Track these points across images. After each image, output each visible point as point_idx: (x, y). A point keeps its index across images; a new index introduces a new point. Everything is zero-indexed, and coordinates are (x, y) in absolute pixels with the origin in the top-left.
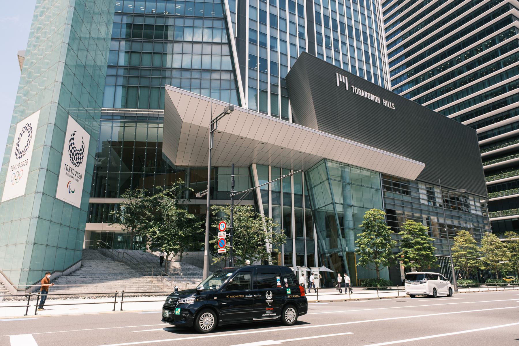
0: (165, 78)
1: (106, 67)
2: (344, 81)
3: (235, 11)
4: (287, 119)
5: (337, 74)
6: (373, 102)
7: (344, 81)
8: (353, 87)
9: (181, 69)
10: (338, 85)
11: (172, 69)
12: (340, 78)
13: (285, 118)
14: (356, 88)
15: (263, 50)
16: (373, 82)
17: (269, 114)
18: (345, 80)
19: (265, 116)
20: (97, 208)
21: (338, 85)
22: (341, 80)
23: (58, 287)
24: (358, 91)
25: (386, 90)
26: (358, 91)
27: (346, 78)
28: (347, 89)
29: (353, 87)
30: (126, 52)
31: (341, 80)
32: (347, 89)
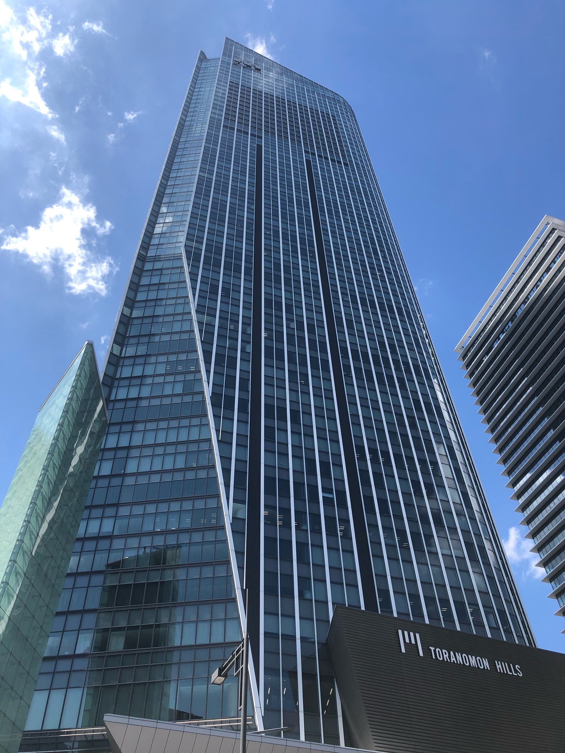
0: (170, 681)
3: (252, 261)
5: (400, 632)
6: (476, 670)
7: (413, 642)
8: (432, 649)
10: (403, 650)
11: (181, 648)
12: (405, 637)
14: (437, 650)
16: (528, 645)
17: (323, 742)
18: (417, 639)
20: (213, 564)
21: (403, 650)
22: (407, 641)
24: (443, 655)
25: (521, 647)
26: (443, 655)
27: (417, 635)
28: (421, 654)
29: (432, 649)
32: (421, 654)
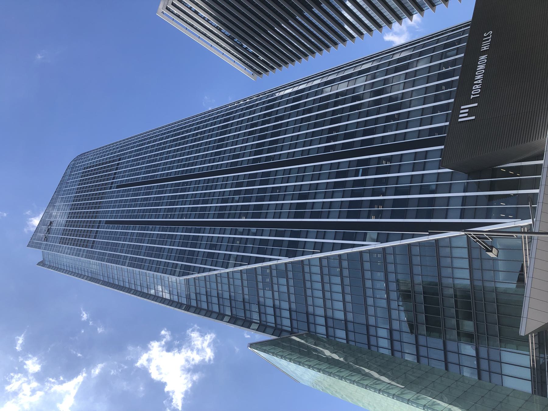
1: (480, 381)
2: (467, 110)
5: (460, 120)
7: (467, 110)
8: (472, 96)
9: (471, 269)
10: (473, 118)
11: (472, 279)
13: (538, 169)
15: (424, 91)
17: (537, 191)
19: (540, 199)
21: (473, 118)
22: (466, 115)
24: (476, 89)
25: (471, 32)
26: (476, 89)
27: (462, 107)
28: (476, 105)
29: (472, 96)
30: (404, 311)
31: (466, 115)
32: (476, 105)
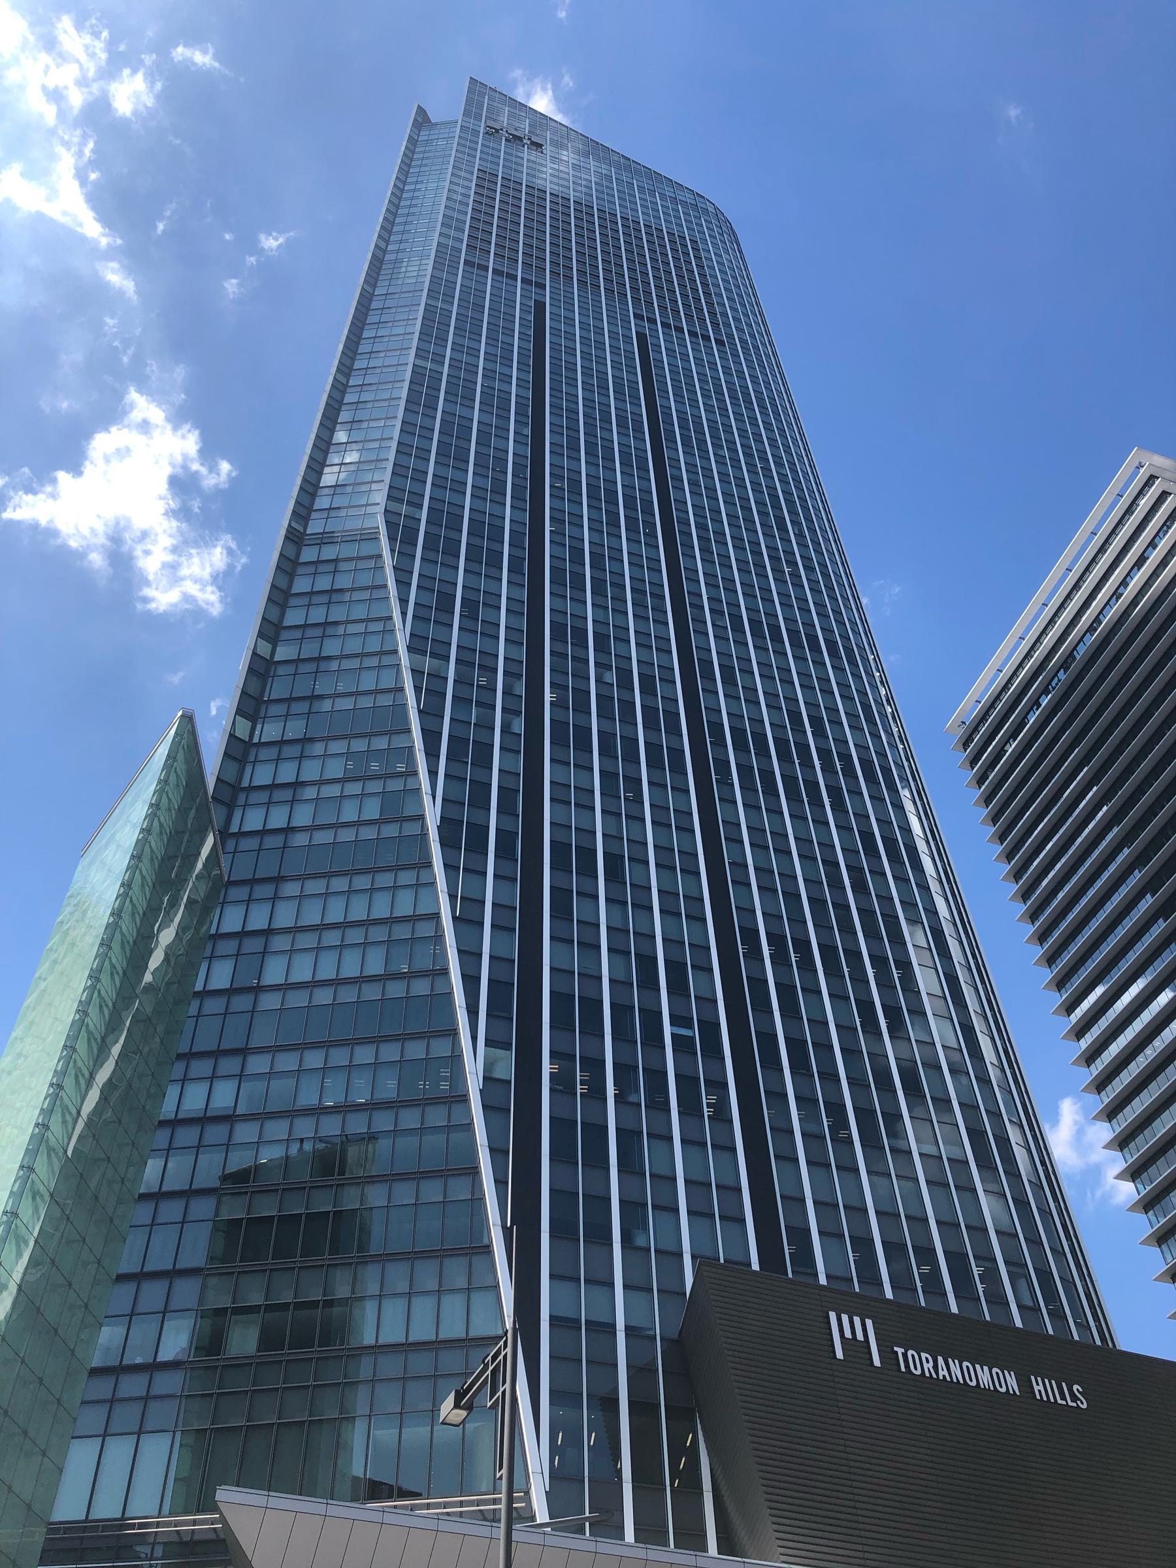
3: (524, 543)
4: (700, 1545)
5: (833, 1316)
6: (990, 1395)
7: (860, 1337)
8: (900, 1351)
10: (840, 1354)
12: (843, 1327)
13: (691, 1538)
16: (1098, 1343)
18: (867, 1330)
19: (607, 1546)
21: (840, 1354)
22: (848, 1334)
23: (361, 1229)
24: (922, 1363)
25: (1085, 1347)
26: (922, 1363)
27: (869, 1322)
28: (877, 1362)
29: (900, 1351)
32: (877, 1362)
